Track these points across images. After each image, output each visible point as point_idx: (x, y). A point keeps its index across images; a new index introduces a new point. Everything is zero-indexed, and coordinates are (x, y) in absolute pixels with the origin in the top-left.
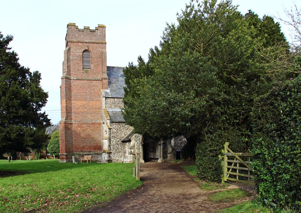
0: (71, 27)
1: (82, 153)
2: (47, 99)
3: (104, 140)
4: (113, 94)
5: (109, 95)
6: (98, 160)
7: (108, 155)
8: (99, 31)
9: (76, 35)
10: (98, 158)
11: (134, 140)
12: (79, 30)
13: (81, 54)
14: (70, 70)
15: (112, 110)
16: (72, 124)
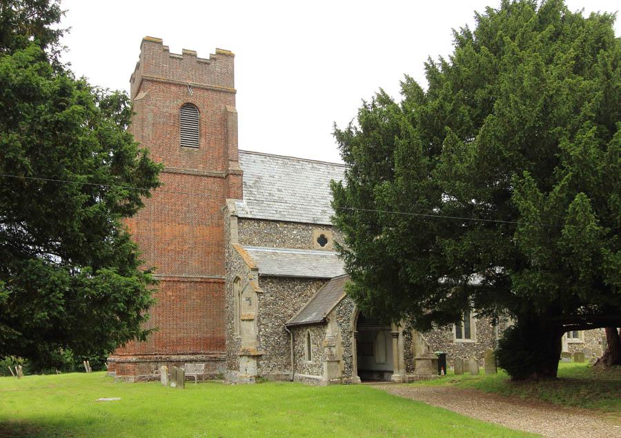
0: (151, 45)
3: (245, 322)
5: (247, 213)
7: (256, 361)
9: (164, 65)
10: (215, 369)
11: (335, 321)
12: (171, 55)
13: (176, 111)
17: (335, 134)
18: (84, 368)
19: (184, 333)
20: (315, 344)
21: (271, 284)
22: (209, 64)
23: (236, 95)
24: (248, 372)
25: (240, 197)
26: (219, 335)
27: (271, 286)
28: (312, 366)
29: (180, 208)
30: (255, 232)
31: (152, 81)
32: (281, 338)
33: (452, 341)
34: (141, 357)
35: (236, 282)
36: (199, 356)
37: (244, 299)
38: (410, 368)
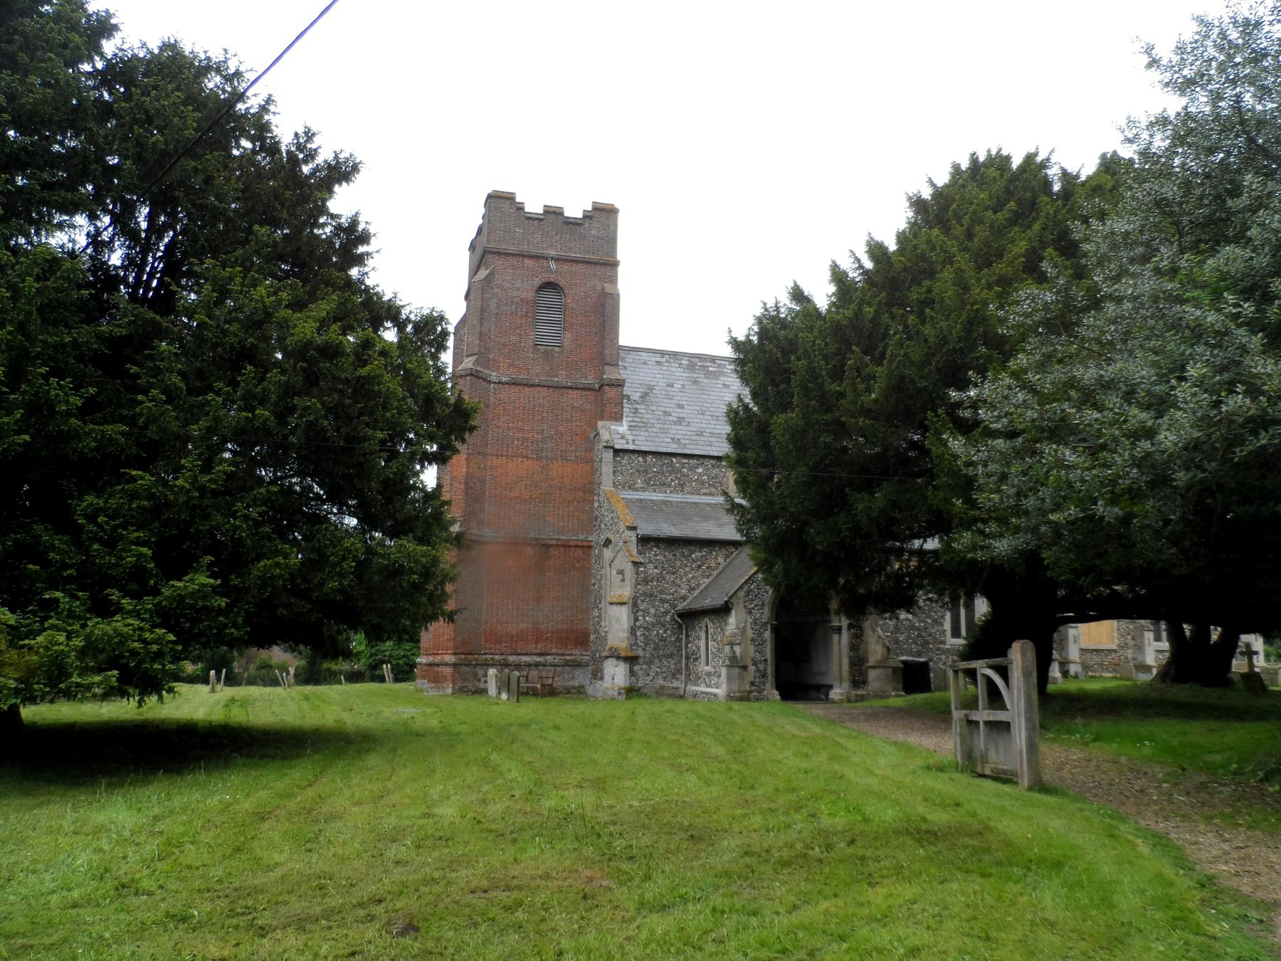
0: (500, 204)
2: (822, 295)
4: (639, 438)
5: (628, 443)
10: (573, 678)
11: (741, 606)
13: (530, 295)
14: (489, 349)
17: (729, 343)
18: (384, 676)
22: (581, 225)
24: (616, 681)
25: (618, 418)
27: (654, 553)
28: (709, 674)
29: (530, 435)
30: (638, 471)
31: (499, 254)
33: (943, 642)
34: (463, 657)
36: (548, 658)
37: (614, 572)
38: (858, 680)
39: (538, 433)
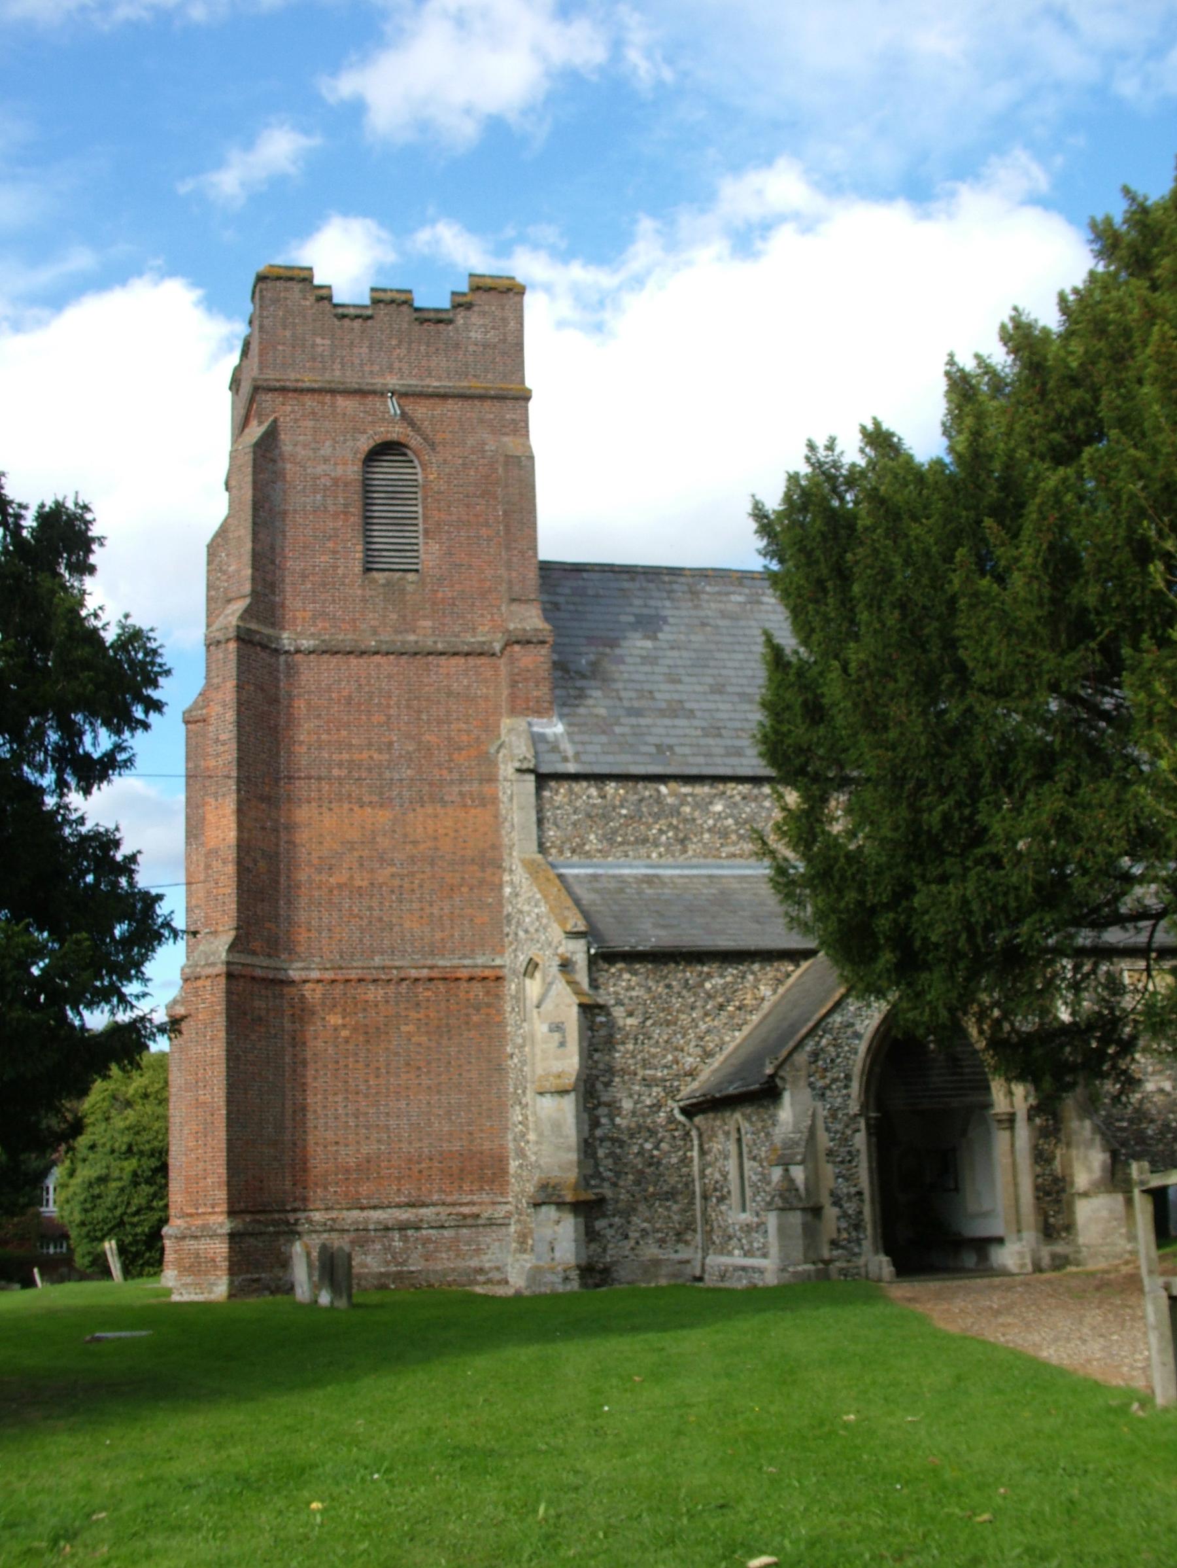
1: (356, 1214)
4: (589, 748)
6: (481, 1271)
8: (475, 318)
9: (319, 341)
10: (478, 1251)
11: (803, 1083)
12: (340, 311)
13: (353, 471)
15: (590, 871)
16: (282, 982)
19: (379, 1141)
20: (754, 1159)
21: (626, 976)
23: (532, 405)
24: (557, 1255)
26: (487, 1145)
29: (365, 755)
30: (589, 816)
31: (283, 390)
32: (664, 1146)
35: (532, 976)
36: (423, 1211)
39: (380, 751)
